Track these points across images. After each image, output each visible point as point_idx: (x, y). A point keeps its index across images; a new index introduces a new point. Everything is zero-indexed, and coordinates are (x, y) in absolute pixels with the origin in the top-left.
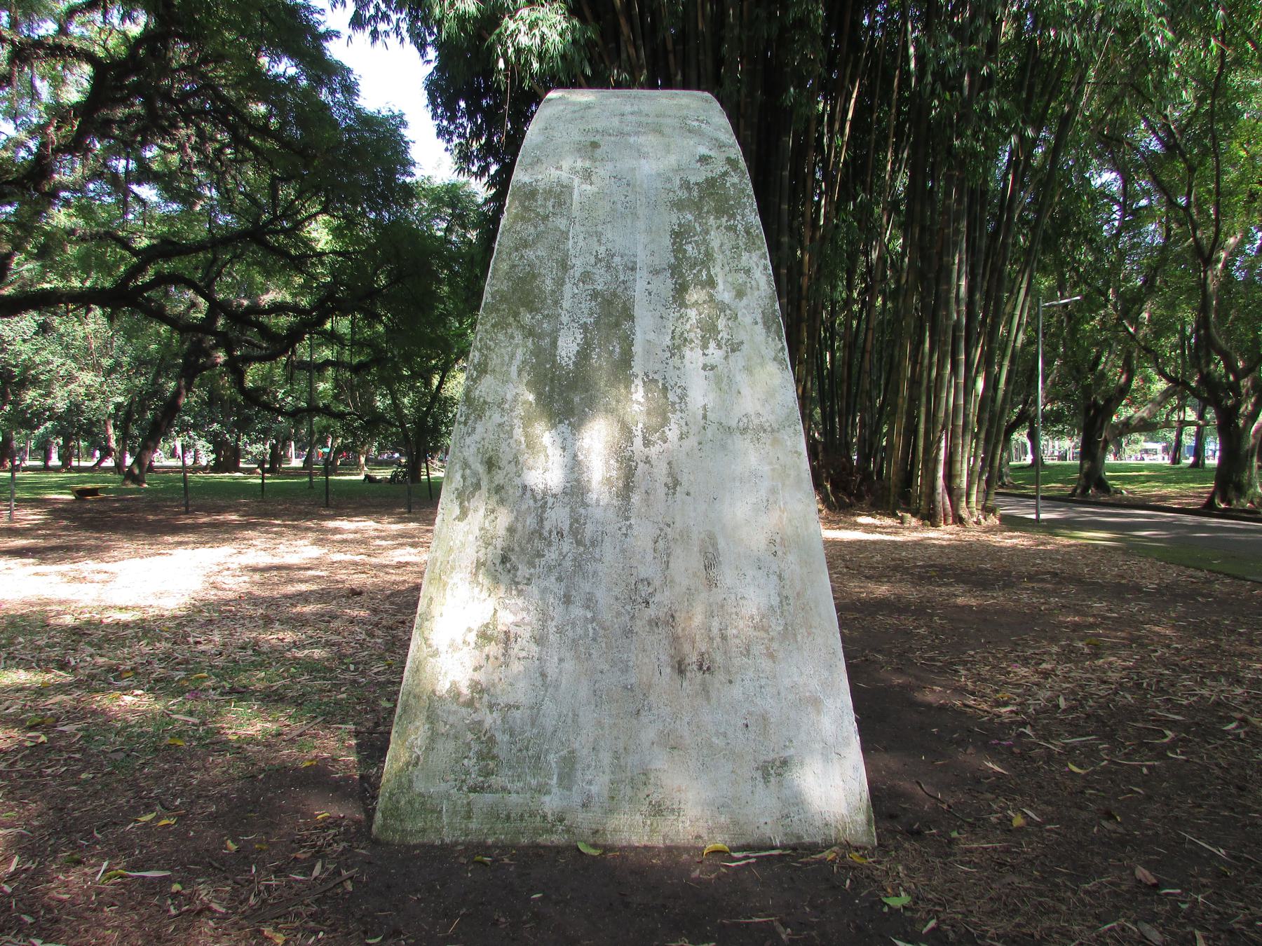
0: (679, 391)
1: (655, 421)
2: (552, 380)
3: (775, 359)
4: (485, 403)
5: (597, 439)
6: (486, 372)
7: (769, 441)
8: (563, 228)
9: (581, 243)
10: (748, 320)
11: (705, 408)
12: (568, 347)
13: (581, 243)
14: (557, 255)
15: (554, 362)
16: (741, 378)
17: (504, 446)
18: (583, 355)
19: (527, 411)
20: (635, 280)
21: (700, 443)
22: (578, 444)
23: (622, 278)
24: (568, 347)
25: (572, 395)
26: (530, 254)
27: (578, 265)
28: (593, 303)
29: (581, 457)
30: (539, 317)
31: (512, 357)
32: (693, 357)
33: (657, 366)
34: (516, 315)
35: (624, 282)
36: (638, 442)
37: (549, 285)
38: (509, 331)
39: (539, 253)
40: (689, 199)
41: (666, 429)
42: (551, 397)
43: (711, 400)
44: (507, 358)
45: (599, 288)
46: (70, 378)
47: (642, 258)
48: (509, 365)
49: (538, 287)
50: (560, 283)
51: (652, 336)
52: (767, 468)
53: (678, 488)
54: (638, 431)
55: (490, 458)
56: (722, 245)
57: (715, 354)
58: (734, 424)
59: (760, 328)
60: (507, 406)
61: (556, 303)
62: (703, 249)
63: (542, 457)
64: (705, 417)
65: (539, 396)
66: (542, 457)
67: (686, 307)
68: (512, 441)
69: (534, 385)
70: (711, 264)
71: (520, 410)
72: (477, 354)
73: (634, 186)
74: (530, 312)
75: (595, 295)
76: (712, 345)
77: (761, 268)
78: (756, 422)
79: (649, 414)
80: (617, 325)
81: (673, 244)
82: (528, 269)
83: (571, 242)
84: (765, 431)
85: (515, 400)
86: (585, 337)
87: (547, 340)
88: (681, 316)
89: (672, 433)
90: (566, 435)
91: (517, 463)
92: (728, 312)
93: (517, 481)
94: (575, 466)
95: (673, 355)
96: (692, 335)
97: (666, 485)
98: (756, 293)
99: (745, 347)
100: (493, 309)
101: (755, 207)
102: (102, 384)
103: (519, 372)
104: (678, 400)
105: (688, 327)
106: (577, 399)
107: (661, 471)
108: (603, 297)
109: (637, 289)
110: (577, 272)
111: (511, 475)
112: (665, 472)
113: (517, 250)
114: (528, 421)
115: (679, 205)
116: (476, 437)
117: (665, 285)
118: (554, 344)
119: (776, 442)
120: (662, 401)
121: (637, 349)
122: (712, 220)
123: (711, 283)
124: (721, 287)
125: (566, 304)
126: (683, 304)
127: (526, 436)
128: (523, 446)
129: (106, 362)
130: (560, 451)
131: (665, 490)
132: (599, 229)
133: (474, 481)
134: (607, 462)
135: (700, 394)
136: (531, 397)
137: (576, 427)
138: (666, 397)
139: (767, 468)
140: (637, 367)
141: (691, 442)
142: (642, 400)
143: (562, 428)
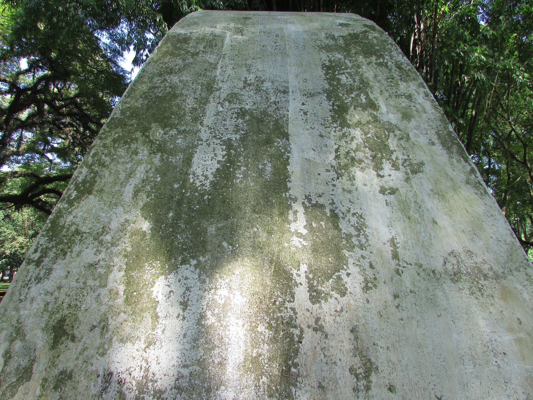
0: (354, 220)
1: (326, 261)
2: (179, 203)
3: (467, 182)
4: (77, 232)
5: (236, 296)
6: (90, 193)
7: (497, 294)
8: (212, 61)
9: (229, 71)
10: (422, 140)
11: (392, 241)
12: (205, 165)
13: (229, 71)
14: (203, 80)
15: (185, 181)
16: (432, 204)
17: (89, 301)
18: (225, 173)
19: (136, 246)
20: (287, 101)
21: (396, 296)
22: (209, 296)
23: (273, 99)
24: (205, 165)
25: (205, 224)
26: (175, 79)
27: (225, 89)
28: (240, 121)
29: (211, 320)
30: (174, 132)
31: (130, 175)
32: (365, 178)
33: (321, 189)
34: (145, 130)
35: (275, 103)
36: (302, 293)
37: (190, 103)
38: (133, 146)
39: (184, 78)
40: (336, 45)
41: (343, 274)
42: (174, 225)
43: (399, 231)
44: (122, 176)
45: (247, 107)
46: (14, 239)
47: (293, 83)
48: (123, 185)
49: (178, 106)
50: (203, 102)
51: (311, 155)
52: (507, 338)
53: (373, 378)
54: (301, 274)
55: (62, 320)
56: (376, 76)
57: (393, 177)
58: (438, 265)
59: (438, 148)
60: (108, 238)
61: (196, 119)
62: (357, 78)
63: (148, 316)
64: (395, 256)
65: (158, 222)
66: (148, 316)
67: (349, 126)
68: (104, 292)
69: (155, 211)
70: (368, 90)
71: (126, 245)
72: (85, 170)
73: (283, 37)
74: (163, 128)
75: (242, 113)
76: (387, 166)
77: (422, 95)
78: (469, 262)
79: (315, 250)
80: (268, 142)
81: (326, 74)
82: (169, 90)
83: (218, 72)
84: (486, 277)
85: (123, 229)
86: (229, 155)
87: (180, 156)
88: (344, 135)
89: (353, 281)
90: (191, 282)
91: (105, 328)
92: (397, 132)
93: (98, 365)
94: (198, 338)
95: (340, 176)
96: (360, 155)
97: (351, 370)
98: (424, 116)
99: (427, 168)
100: (120, 123)
101: (400, 50)
102: (27, 243)
103: (136, 193)
104: (355, 233)
105: (354, 146)
106: (212, 230)
107: (342, 346)
108: (251, 115)
109: (290, 108)
110: (225, 89)
111: (91, 351)
112: (347, 346)
113: (160, 75)
114: (134, 262)
115: (328, 49)
116: (48, 285)
117: (323, 107)
118: (188, 162)
119: (507, 294)
120: (332, 233)
121: (294, 168)
122: (361, 58)
123: (372, 105)
124: (383, 109)
125: (208, 120)
126: (344, 124)
127: (128, 284)
128: (120, 301)
129: (31, 232)
130: (177, 310)
131: (351, 380)
132: (249, 62)
133: (24, 362)
134: (253, 329)
135: (382, 226)
136: (146, 226)
137: (208, 271)
138: (337, 227)
139: (506, 339)
140: (296, 187)
141: (383, 294)
142: (304, 232)
143: (186, 271)
